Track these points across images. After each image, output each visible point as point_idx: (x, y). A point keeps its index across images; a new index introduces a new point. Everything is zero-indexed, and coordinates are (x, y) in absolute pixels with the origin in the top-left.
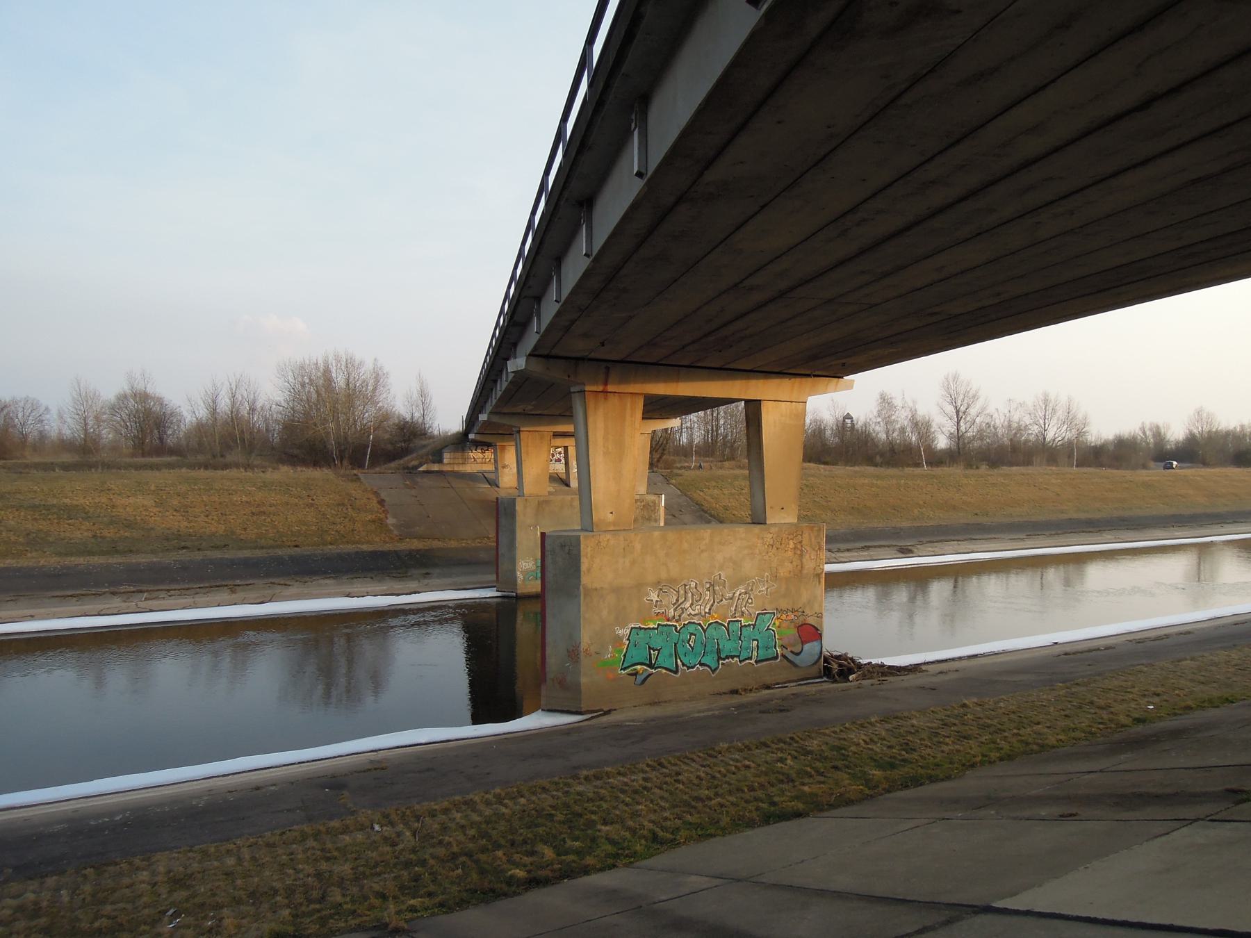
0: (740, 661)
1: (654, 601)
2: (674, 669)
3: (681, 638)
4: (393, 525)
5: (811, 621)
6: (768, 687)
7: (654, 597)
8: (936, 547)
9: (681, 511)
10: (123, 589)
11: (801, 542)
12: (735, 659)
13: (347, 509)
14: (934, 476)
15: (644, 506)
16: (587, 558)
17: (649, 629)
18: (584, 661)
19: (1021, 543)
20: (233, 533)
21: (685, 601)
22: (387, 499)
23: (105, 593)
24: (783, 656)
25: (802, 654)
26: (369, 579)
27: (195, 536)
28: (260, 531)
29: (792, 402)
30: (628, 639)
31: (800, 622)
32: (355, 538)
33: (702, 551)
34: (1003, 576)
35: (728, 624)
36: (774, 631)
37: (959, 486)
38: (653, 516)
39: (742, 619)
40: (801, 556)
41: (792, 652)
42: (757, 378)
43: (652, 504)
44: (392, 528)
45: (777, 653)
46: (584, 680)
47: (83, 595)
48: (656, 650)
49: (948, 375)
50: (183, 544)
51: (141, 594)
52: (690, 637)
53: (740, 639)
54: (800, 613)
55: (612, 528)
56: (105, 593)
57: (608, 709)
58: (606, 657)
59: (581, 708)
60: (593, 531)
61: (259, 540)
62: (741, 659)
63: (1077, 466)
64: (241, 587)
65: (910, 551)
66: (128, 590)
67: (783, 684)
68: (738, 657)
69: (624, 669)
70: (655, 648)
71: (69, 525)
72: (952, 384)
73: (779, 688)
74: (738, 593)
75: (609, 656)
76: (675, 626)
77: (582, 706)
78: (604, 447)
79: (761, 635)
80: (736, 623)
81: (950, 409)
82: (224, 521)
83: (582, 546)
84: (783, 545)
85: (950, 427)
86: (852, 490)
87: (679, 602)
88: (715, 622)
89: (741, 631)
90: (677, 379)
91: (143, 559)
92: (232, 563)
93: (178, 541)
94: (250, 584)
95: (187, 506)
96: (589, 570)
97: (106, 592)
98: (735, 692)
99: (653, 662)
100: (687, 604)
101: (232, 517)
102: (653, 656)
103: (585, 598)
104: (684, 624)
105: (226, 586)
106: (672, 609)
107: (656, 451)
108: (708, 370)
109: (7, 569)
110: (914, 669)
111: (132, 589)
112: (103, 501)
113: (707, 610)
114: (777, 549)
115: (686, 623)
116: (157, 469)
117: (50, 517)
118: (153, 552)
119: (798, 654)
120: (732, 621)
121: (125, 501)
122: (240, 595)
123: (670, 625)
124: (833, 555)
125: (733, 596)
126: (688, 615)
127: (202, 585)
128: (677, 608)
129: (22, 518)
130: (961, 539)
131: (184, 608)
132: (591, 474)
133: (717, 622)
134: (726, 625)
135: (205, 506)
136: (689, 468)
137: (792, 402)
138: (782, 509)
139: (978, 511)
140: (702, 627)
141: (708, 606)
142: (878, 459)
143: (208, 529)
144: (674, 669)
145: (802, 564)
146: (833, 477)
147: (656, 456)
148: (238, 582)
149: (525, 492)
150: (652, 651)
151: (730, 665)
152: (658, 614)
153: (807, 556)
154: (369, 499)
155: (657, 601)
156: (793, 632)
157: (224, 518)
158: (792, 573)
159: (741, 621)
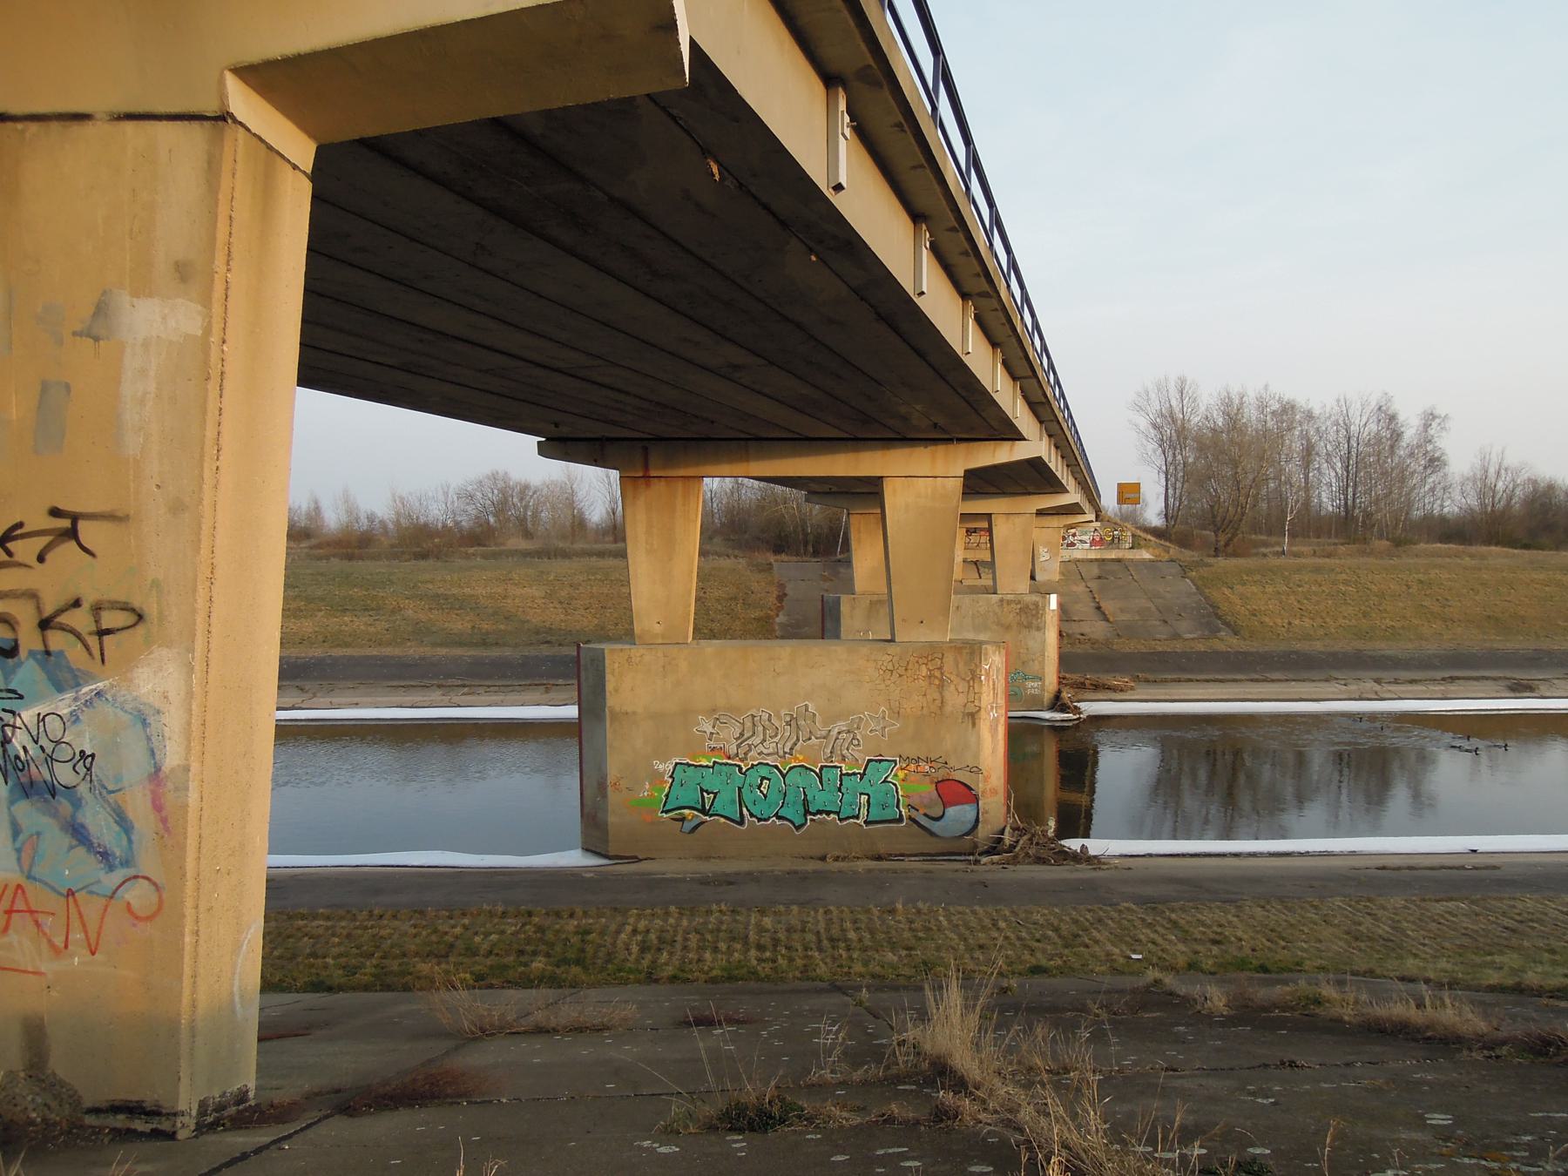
0: (840, 820)
1: (708, 734)
2: (738, 820)
3: (748, 781)
6: (879, 858)
9: (1180, 615)
10: (450, 682)
11: (940, 668)
12: (832, 816)
16: (613, 675)
17: (700, 766)
21: (752, 736)
24: (910, 818)
25: (943, 820)
30: (671, 777)
31: (941, 775)
36: (895, 785)
38: (1034, 622)
39: (843, 765)
40: (941, 687)
41: (925, 815)
42: (870, 449)
43: (1031, 607)
46: (612, 819)
48: (712, 793)
52: (762, 781)
54: (940, 765)
55: (660, 641)
57: (645, 857)
59: (608, 851)
68: (838, 813)
70: (710, 791)
71: (457, 615)
74: (836, 730)
76: (739, 766)
77: (610, 849)
78: (647, 543)
79: (873, 788)
80: (834, 770)
83: (607, 662)
87: (745, 737)
88: (799, 766)
89: (841, 780)
91: (495, 653)
93: (545, 635)
95: (572, 598)
96: (616, 690)
99: (707, 808)
100: (757, 740)
102: (706, 801)
103: (611, 725)
104: (752, 764)
106: (734, 747)
113: (787, 750)
114: (900, 676)
115: (755, 763)
119: (938, 819)
120: (826, 766)
121: (519, 591)
122: (552, 695)
126: (759, 754)
128: (741, 743)
131: (489, 706)
133: (802, 766)
134: (817, 771)
138: (922, 622)
141: (789, 745)
144: (738, 820)
145: (942, 697)
148: (560, 681)
150: (705, 794)
151: (823, 822)
153: (952, 687)
155: (712, 733)
156: (927, 789)
159: (841, 767)
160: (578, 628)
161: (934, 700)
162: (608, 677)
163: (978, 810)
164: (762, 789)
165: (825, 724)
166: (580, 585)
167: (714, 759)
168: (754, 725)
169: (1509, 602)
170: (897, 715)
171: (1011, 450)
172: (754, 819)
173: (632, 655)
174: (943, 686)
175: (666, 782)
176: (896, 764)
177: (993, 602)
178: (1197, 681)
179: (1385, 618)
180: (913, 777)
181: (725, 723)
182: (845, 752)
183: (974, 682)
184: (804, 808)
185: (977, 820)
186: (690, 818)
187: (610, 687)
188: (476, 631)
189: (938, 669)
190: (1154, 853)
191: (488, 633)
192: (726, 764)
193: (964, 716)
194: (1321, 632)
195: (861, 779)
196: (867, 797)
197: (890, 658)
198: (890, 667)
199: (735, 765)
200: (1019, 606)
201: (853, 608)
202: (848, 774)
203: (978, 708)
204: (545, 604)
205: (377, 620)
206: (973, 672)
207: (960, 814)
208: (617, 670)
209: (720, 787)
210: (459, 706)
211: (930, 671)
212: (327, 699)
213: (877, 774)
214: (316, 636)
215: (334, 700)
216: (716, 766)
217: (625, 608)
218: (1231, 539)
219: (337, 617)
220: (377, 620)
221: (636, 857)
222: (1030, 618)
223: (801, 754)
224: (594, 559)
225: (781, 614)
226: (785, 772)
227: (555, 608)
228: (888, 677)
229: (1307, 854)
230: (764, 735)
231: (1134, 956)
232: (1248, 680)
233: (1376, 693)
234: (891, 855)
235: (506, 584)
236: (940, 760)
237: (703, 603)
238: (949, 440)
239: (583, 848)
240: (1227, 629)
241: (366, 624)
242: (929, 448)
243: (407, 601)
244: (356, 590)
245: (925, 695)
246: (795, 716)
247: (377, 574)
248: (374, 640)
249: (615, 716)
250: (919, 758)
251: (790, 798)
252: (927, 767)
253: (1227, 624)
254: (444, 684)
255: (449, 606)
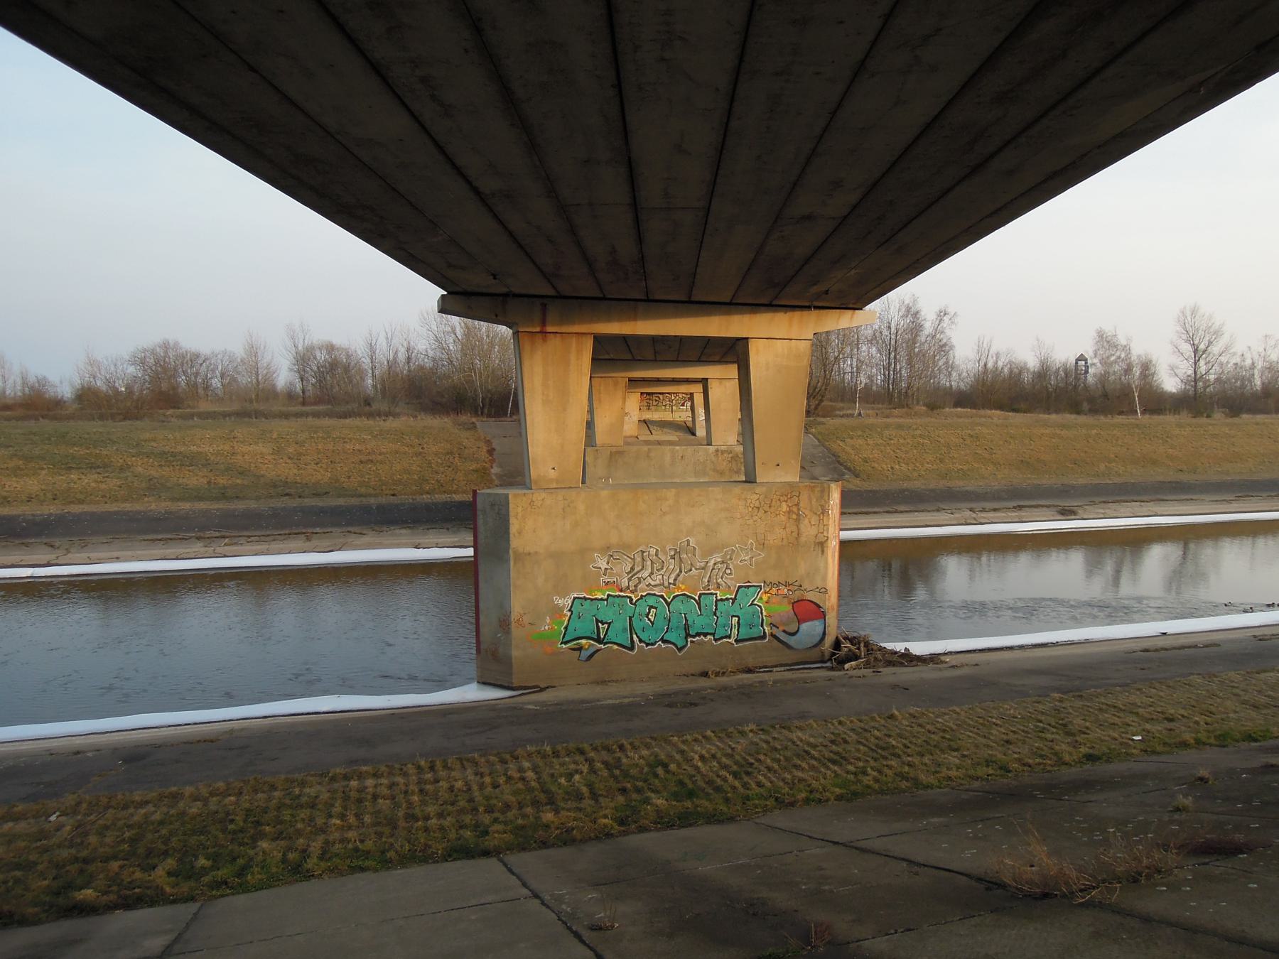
0: (715, 640)
1: (603, 569)
2: (630, 646)
3: (637, 611)
4: (496, 474)
5: (811, 596)
6: (749, 671)
7: (603, 564)
8: (1109, 508)
9: (813, 462)
10: (208, 534)
11: (797, 505)
12: (709, 637)
13: (454, 457)
14: (1137, 425)
15: (732, 458)
17: (596, 599)
18: (516, 631)
19: (1226, 506)
20: (337, 481)
21: (642, 569)
22: (498, 448)
23: (191, 538)
24: (772, 635)
25: (798, 634)
26: (445, 530)
27: (300, 483)
28: (363, 479)
29: (791, 339)
30: (570, 610)
31: (797, 596)
32: (452, 487)
33: (665, 514)
34: (1248, 542)
35: (700, 597)
36: (760, 607)
37: (1167, 437)
39: (718, 592)
40: (798, 521)
41: (784, 631)
44: (494, 478)
45: (764, 633)
46: (515, 653)
47: (171, 539)
48: (606, 623)
49: (1185, 308)
50: (287, 491)
51: (223, 539)
53: (715, 614)
56: (191, 538)
57: (546, 686)
58: (543, 629)
59: (512, 683)
60: (531, 489)
61: (359, 488)
62: (716, 637)
63: (1143, 413)
64: (318, 535)
65: (1074, 513)
66: (211, 535)
67: (768, 668)
68: (713, 634)
69: (566, 643)
71: (189, 471)
72: (1190, 319)
73: (764, 672)
74: (713, 562)
75: (547, 628)
76: (630, 597)
78: (543, 394)
80: (711, 597)
81: (1187, 349)
82: (332, 469)
84: (773, 508)
85: (1186, 369)
86: (1027, 441)
87: (635, 571)
88: (681, 595)
89: (716, 606)
90: (634, 317)
91: (241, 506)
92: (322, 511)
93: (283, 488)
94: (328, 532)
95: (300, 454)
97: (193, 536)
98: (705, 674)
99: (602, 637)
100: (646, 574)
101: (340, 465)
102: (601, 631)
103: (515, 563)
105: (304, 533)
106: (626, 579)
107: (814, 398)
108: (698, 305)
109: (10, 519)
110: (934, 659)
111: (217, 534)
112: (226, 448)
113: (671, 581)
114: (765, 512)
116: (286, 418)
117: (174, 463)
118: (258, 498)
121: (246, 449)
122: (315, 542)
123: (624, 596)
124: (974, 515)
125: (706, 565)
126: (647, 586)
127: (282, 532)
128: (632, 577)
129: (149, 464)
130: (1145, 500)
131: (256, 555)
132: (528, 426)
133: (684, 595)
134: (697, 598)
135: (318, 453)
136: (852, 415)
137: (791, 339)
138: (778, 465)
139: (1185, 468)
140: (694, 599)
141: (673, 576)
142: (1085, 406)
143: (315, 477)
144: (630, 646)
145: (799, 529)
146: (1007, 426)
147: (814, 403)
148: (318, 530)
149: (597, 443)
152: (607, 583)
153: (806, 521)
154: (479, 448)
155: (606, 569)
156: (786, 608)
157: (332, 466)
158: (785, 541)
159: (716, 594)
160: (313, 481)
161: (792, 532)
162: (512, 520)
163: (825, 625)
164: (650, 617)
165: (705, 555)
166: (304, 442)
167: (608, 593)
168: (643, 560)
169: (1032, 450)
170: (762, 546)
171: (852, 318)
172: (643, 644)
173: (534, 499)
174: (799, 520)
175: (565, 615)
176: (761, 589)
177: (710, 451)
178: (849, 513)
179: (955, 463)
180: (775, 599)
181: (618, 559)
182: (720, 580)
183: (823, 516)
184: (686, 632)
185: (824, 633)
186: (587, 647)
187: (514, 529)
188: (212, 486)
189: (796, 505)
190: (953, 650)
191: (225, 488)
192: (619, 596)
193: (815, 545)
194: (915, 474)
195: (733, 603)
196: (737, 619)
197: (757, 497)
198: (757, 505)
199: (627, 596)
200: (730, 455)
201: (596, 459)
202: (721, 600)
203: (826, 538)
204: (275, 459)
205: (107, 477)
206: (823, 507)
207: (811, 629)
208: (520, 515)
209: (613, 617)
210: (225, 556)
211: (789, 507)
212: (83, 555)
213: (747, 598)
214: (45, 494)
215: (91, 555)
216: (610, 599)
217: (353, 462)
218: (818, 405)
219: (62, 475)
220: (107, 477)
221: (537, 687)
222: (739, 464)
223: (682, 584)
224: (310, 419)
225: (494, 465)
226: (670, 600)
227: (286, 463)
228: (756, 514)
229: (1071, 643)
230: (652, 568)
231: (1135, 738)
232: (884, 512)
233: (975, 519)
234: (756, 667)
235: (232, 441)
236: (796, 584)
237: (424, 457)
238: (808, 308)
239: (478, 682)
240: (849, 473)
241: (96, 481)
242: (788, 314)
243: (134, 459)
244: (76, 449)
245: (785, 528)
246: (678, 551)
247: (95, 433)
248: (108, 496)
249: (519, 557)
250: (779, 582)
251: (674, 623)
252: (786, 590)
253: (849, 469)
254: (202, 535)
255: (179, 463)
